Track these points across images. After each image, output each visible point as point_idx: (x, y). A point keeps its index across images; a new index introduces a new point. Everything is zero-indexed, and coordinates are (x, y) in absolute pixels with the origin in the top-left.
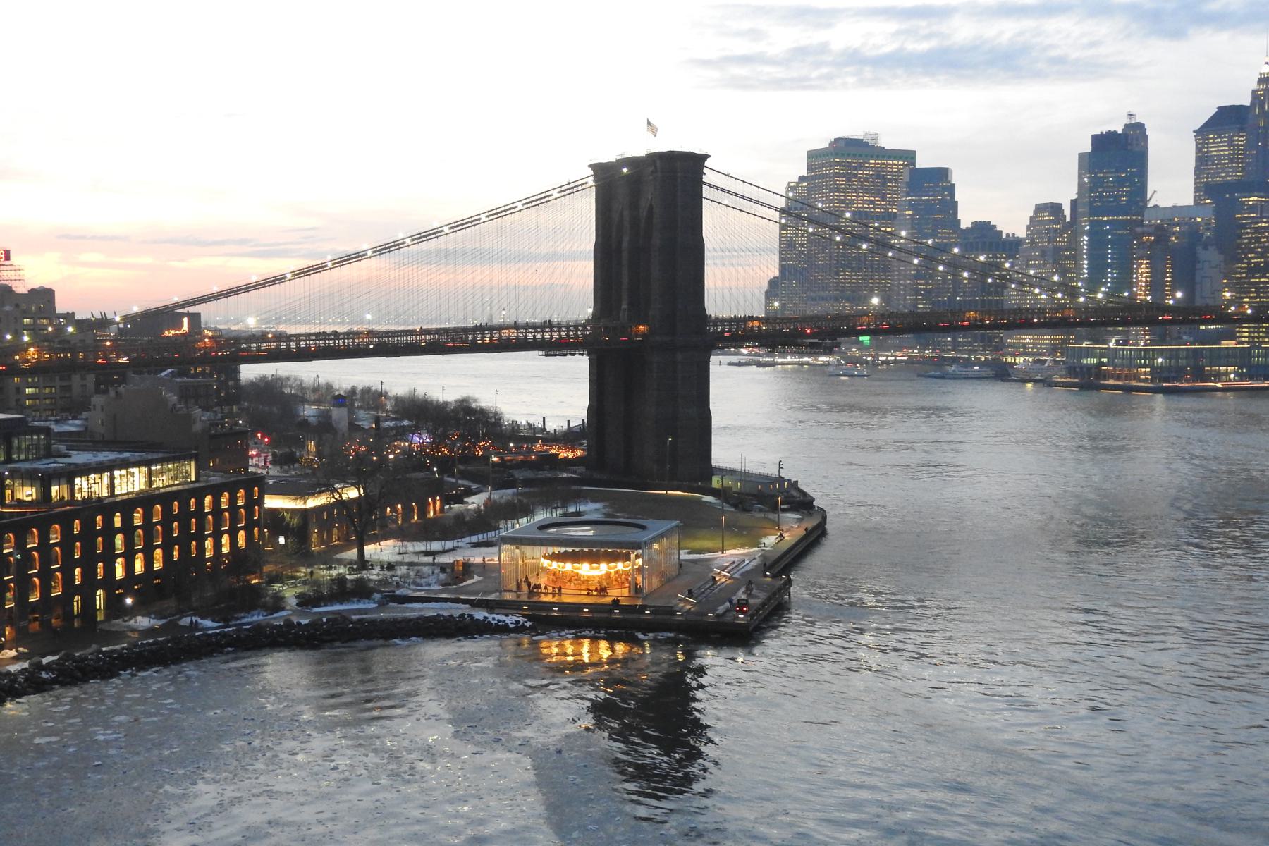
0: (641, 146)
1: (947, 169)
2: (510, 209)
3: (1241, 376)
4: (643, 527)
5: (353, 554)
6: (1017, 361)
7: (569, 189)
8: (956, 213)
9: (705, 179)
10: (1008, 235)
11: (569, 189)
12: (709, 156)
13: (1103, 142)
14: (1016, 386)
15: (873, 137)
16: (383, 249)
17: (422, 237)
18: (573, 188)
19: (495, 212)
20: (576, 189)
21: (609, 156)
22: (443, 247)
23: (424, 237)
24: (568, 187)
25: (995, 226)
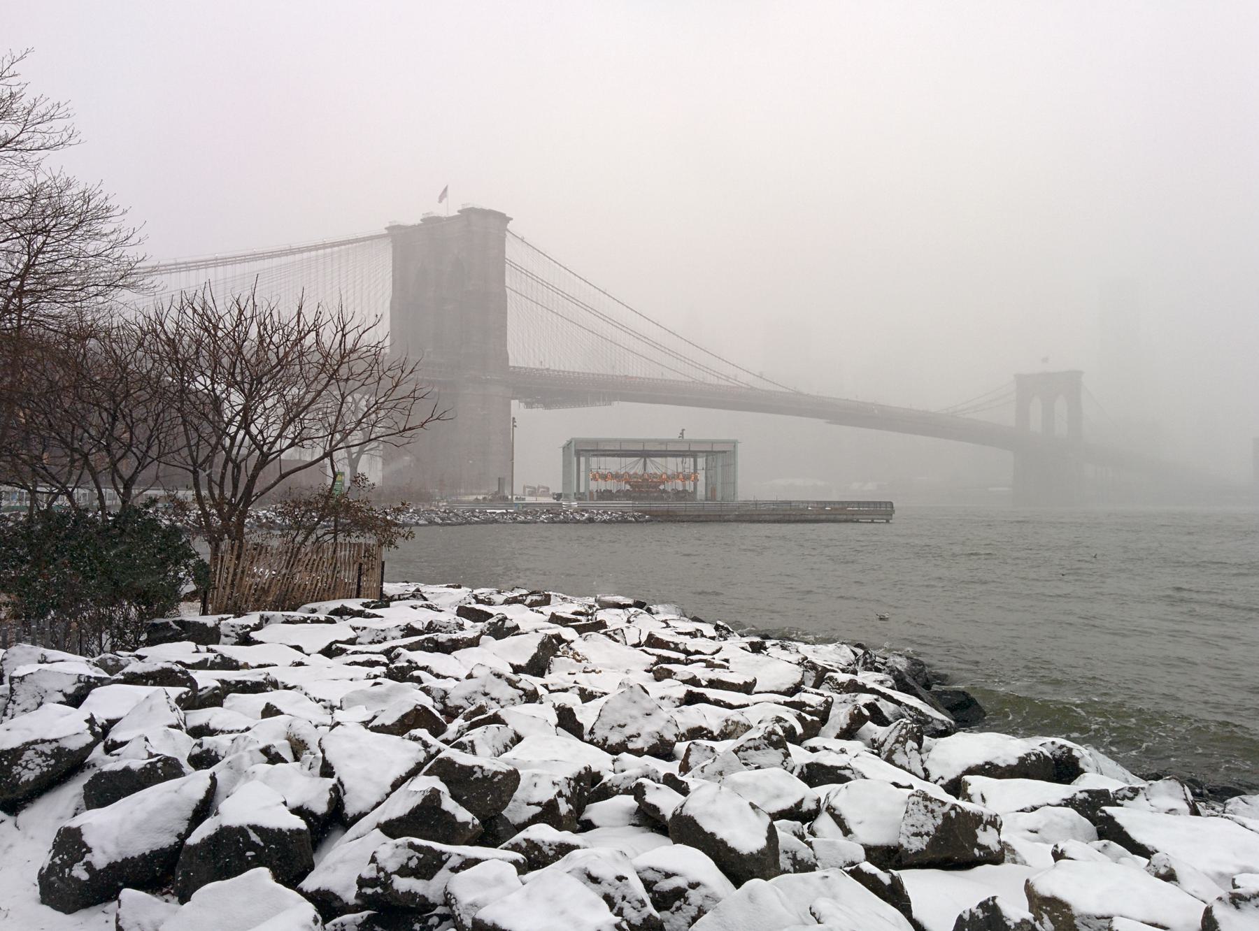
12: (511, 219)
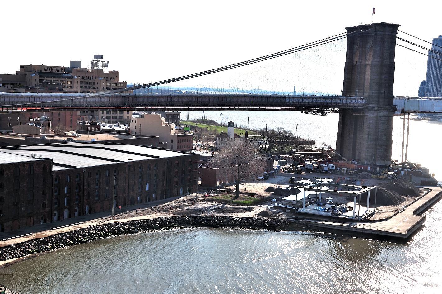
0: (368, 20)
2: (310, 46)
5: (233, 187)
6: (167, 99)
7: (336, 38)
9: (397, 35)
11: (336, 38)
12: (398, 26)
16: (266, 58)
17: (263, 59)
18: (337, 37)
19: (303, 47)
20: (339, 38)
21: (355, 24)
22: (161, 87)
23: (264, 58)
24: (335, 37)
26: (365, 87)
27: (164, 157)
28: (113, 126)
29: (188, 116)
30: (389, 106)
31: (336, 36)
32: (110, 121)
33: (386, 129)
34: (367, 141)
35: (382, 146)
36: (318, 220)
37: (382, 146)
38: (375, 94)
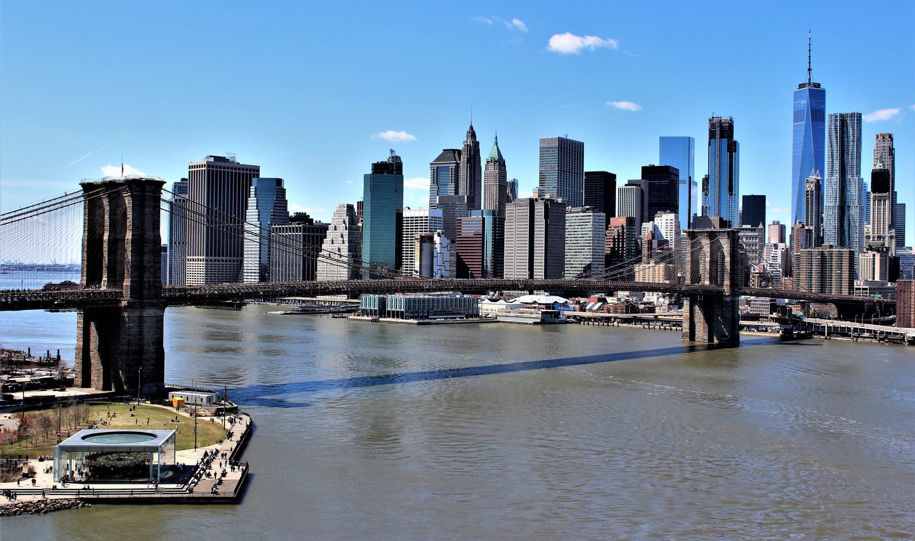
1: (281, 179)
3: (869, 223)
4: (154, 436)
8: (286, 207)
10: (316, 222)
12: (165, 182)
13: (379, 168)
14: (443, 327)
15: (233, 156)
25: (309, 216)
26: (118, 273)
27: (42, 311)
28: (119, 212)
29: (252, 191)
30: (157, 300)
31: (66, 195)
32: (221, 168)
33: (154, 335)
34: (127, 355)
35: (150, 360)
36: (723, 270)
37: (150, 360)
38: (135, 284)
